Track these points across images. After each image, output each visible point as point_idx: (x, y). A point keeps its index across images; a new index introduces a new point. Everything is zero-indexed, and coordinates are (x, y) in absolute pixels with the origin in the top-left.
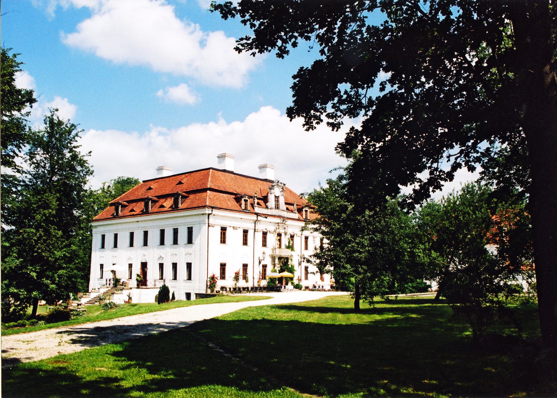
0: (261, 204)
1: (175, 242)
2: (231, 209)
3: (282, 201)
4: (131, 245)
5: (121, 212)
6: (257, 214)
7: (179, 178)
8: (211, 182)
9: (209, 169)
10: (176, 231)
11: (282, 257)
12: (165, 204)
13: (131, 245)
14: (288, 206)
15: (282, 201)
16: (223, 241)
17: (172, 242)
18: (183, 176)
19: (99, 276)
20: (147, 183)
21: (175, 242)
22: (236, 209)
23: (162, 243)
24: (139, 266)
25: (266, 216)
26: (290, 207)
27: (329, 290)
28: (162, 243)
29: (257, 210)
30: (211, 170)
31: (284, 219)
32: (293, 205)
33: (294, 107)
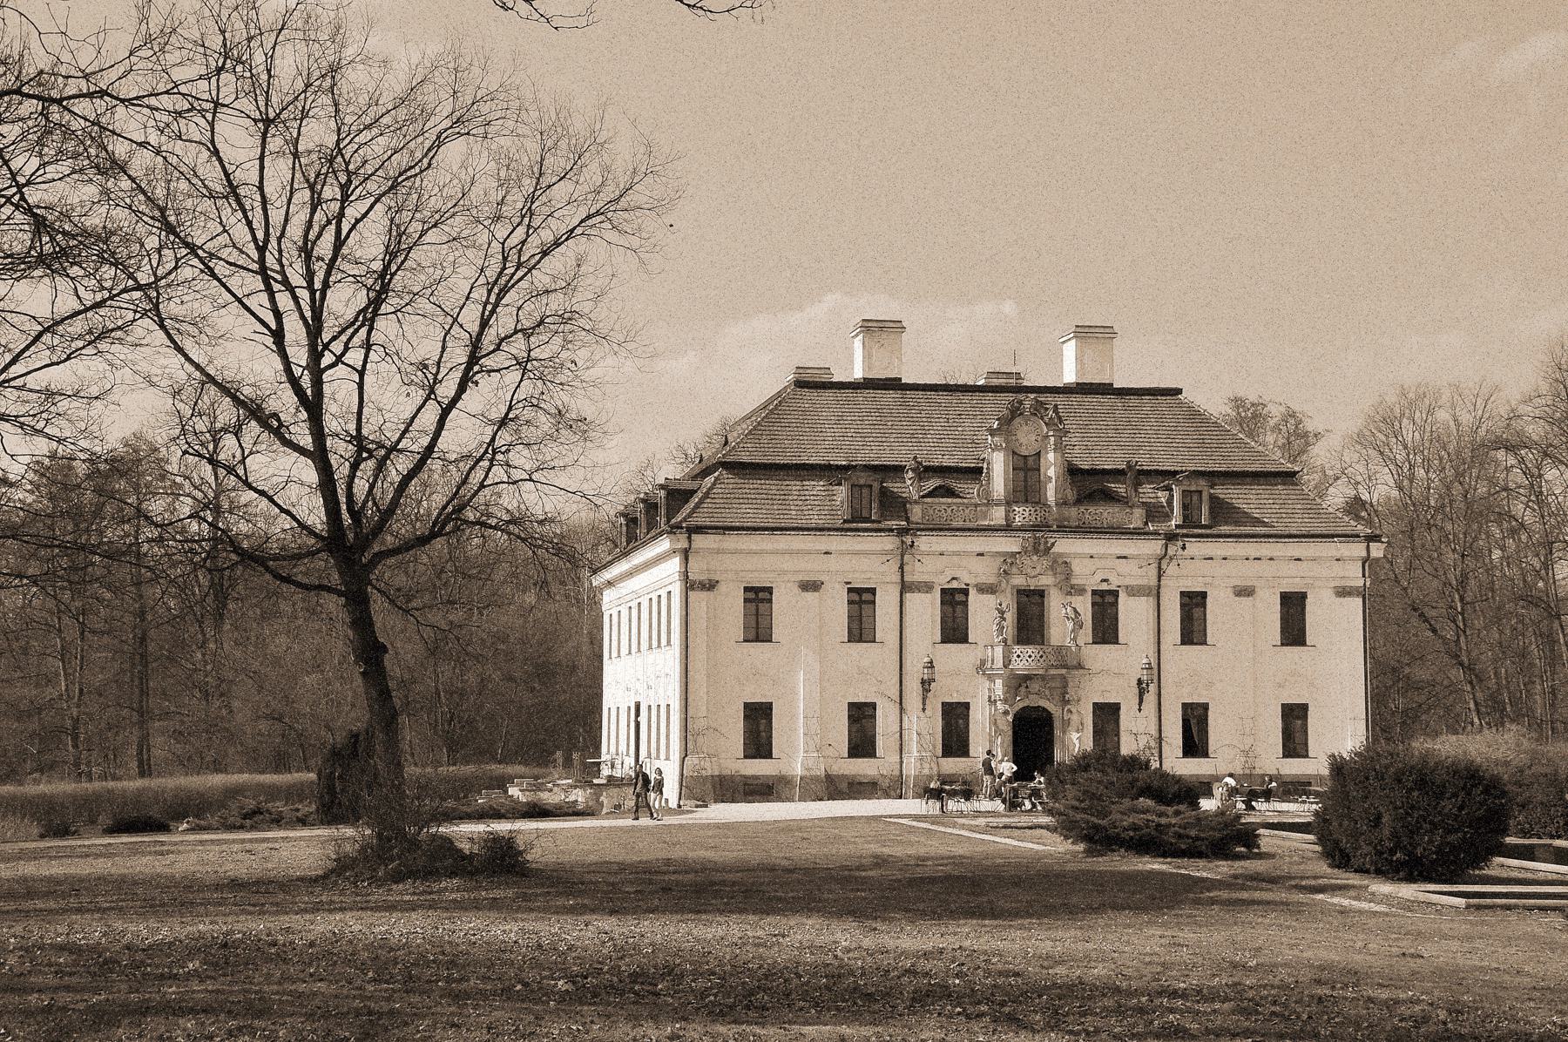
15: (1051, 466)
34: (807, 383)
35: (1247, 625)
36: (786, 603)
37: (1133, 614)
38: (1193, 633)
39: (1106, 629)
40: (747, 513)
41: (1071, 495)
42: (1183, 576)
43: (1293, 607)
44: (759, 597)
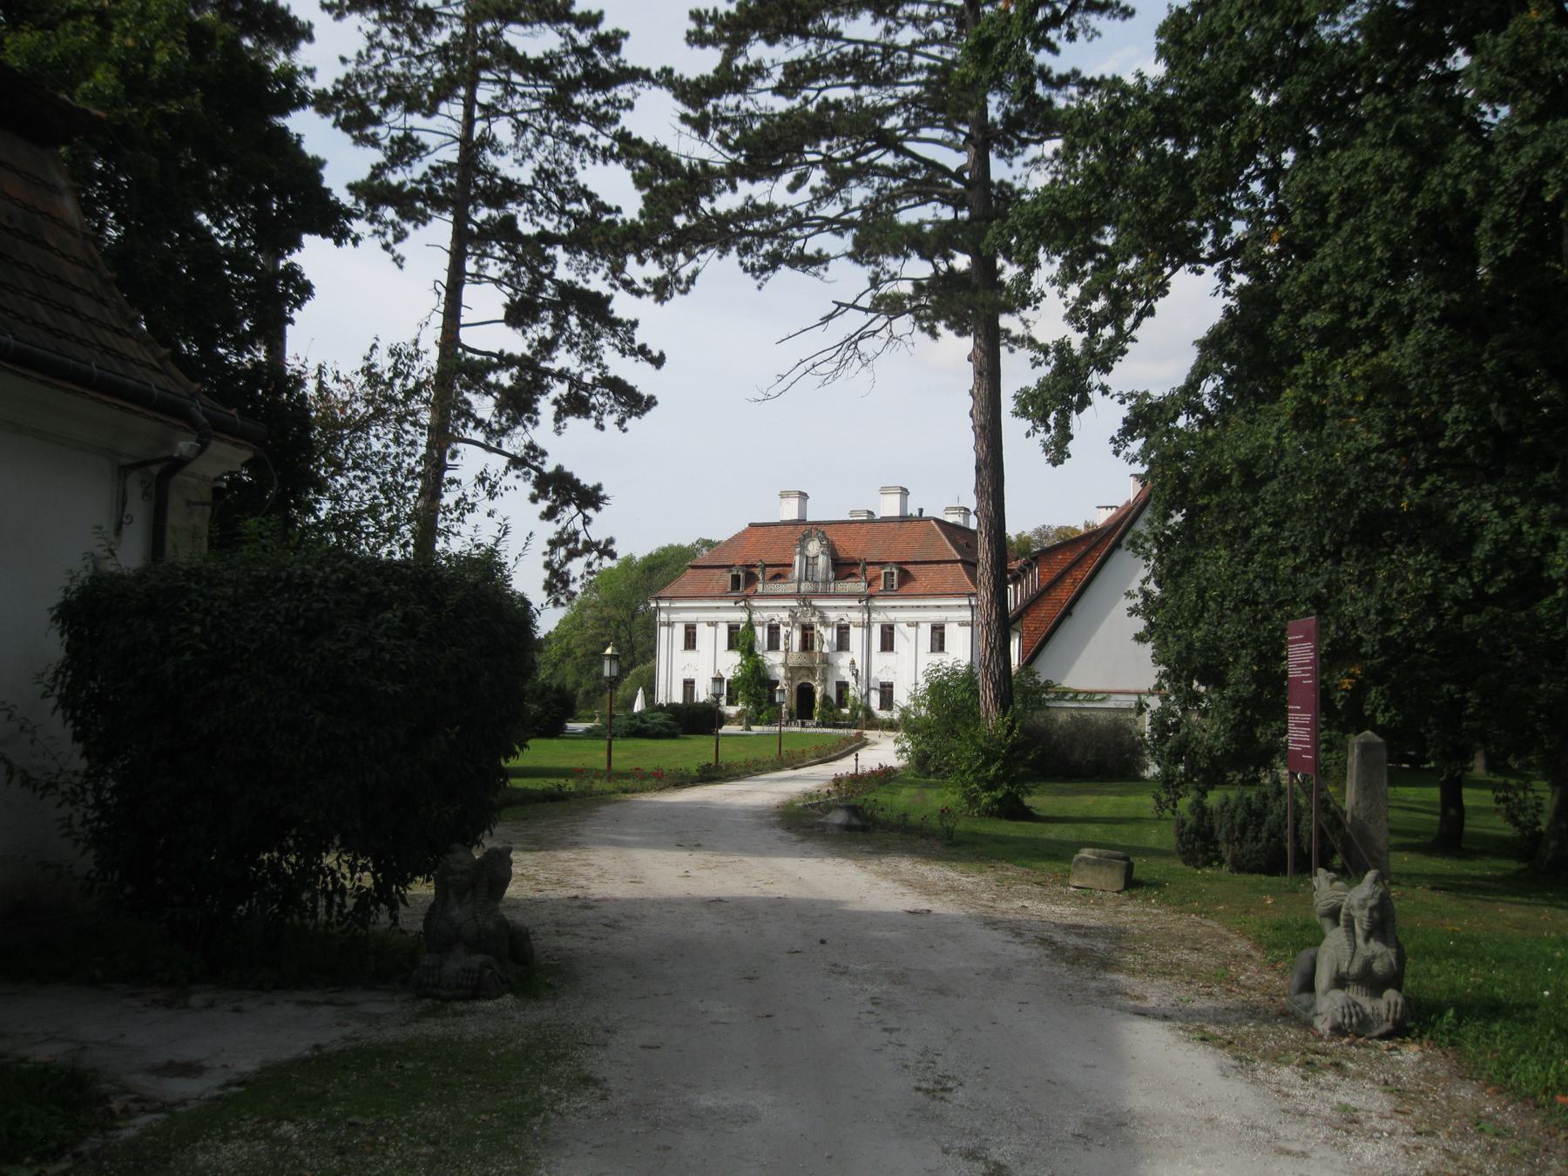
15: (822, 561)
34: (752, 525)
36: (703, 633)
37: (856, 635)
38: (887, 645)
39: (843, 644)
41: (831, 575)
43: (938, 632)
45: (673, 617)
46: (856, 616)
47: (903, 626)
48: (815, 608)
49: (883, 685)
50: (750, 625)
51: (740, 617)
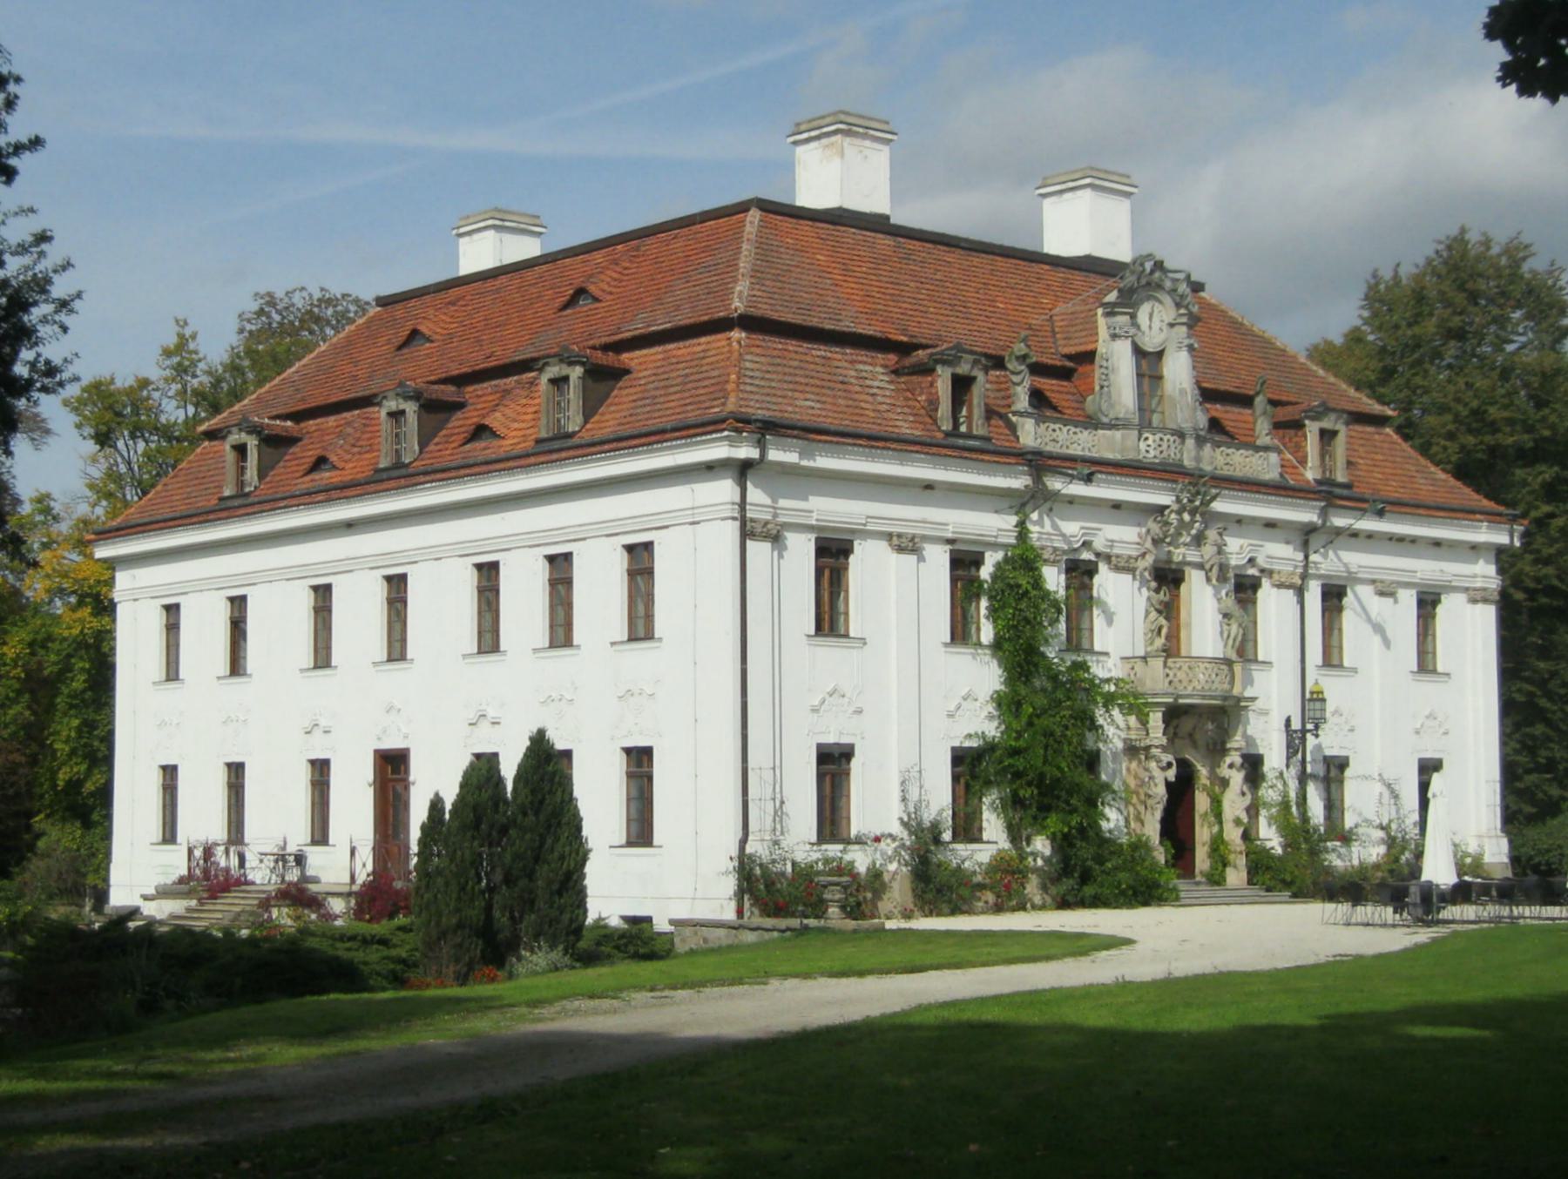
0: (1054, 398)
1: (561, 633)
2: (1430, 501)
3: (1178, 371)
4: (322, 657)
5: (262, 475)
6: (1039, 463)
7: (576, 271)
8: (756, 275)
9: (742, 208)
10: (560, 567)
11: (1188, 710)
12: (495, 421)
13: (322, 657)
14: (1218, 410)
15: (1178, 371)
16: (829, 619)
17: (541, 636)
18: (598, 257)
19: (155, 831)
20: (398, 311)
21: (561, 633)
22: (1455, 503)
23: (489, 639)
24: (366, 771)
25: (1091, 468)
26: (1230, 415)
27: (925, 538)
28: (489, 639)
29: (1030, 434)
30: (754, 215)
31: (1199, 485)
32: (1246, 401)
33: (337, 917)
35: (1378, 627)
36: (869, 566)
40: (805, 408)
42: (1330, 562)
44: (833, 554)
45: (790, 506)
46: (1280, 554)
47: (1365, 592)
48: (1210, 518)
49: (1328, 761)
50: (1024, 560)
51: (995, 525)
